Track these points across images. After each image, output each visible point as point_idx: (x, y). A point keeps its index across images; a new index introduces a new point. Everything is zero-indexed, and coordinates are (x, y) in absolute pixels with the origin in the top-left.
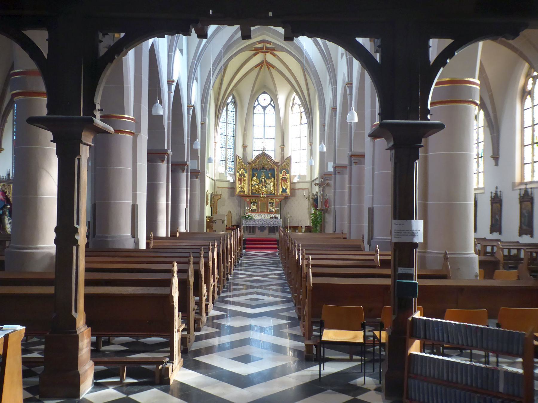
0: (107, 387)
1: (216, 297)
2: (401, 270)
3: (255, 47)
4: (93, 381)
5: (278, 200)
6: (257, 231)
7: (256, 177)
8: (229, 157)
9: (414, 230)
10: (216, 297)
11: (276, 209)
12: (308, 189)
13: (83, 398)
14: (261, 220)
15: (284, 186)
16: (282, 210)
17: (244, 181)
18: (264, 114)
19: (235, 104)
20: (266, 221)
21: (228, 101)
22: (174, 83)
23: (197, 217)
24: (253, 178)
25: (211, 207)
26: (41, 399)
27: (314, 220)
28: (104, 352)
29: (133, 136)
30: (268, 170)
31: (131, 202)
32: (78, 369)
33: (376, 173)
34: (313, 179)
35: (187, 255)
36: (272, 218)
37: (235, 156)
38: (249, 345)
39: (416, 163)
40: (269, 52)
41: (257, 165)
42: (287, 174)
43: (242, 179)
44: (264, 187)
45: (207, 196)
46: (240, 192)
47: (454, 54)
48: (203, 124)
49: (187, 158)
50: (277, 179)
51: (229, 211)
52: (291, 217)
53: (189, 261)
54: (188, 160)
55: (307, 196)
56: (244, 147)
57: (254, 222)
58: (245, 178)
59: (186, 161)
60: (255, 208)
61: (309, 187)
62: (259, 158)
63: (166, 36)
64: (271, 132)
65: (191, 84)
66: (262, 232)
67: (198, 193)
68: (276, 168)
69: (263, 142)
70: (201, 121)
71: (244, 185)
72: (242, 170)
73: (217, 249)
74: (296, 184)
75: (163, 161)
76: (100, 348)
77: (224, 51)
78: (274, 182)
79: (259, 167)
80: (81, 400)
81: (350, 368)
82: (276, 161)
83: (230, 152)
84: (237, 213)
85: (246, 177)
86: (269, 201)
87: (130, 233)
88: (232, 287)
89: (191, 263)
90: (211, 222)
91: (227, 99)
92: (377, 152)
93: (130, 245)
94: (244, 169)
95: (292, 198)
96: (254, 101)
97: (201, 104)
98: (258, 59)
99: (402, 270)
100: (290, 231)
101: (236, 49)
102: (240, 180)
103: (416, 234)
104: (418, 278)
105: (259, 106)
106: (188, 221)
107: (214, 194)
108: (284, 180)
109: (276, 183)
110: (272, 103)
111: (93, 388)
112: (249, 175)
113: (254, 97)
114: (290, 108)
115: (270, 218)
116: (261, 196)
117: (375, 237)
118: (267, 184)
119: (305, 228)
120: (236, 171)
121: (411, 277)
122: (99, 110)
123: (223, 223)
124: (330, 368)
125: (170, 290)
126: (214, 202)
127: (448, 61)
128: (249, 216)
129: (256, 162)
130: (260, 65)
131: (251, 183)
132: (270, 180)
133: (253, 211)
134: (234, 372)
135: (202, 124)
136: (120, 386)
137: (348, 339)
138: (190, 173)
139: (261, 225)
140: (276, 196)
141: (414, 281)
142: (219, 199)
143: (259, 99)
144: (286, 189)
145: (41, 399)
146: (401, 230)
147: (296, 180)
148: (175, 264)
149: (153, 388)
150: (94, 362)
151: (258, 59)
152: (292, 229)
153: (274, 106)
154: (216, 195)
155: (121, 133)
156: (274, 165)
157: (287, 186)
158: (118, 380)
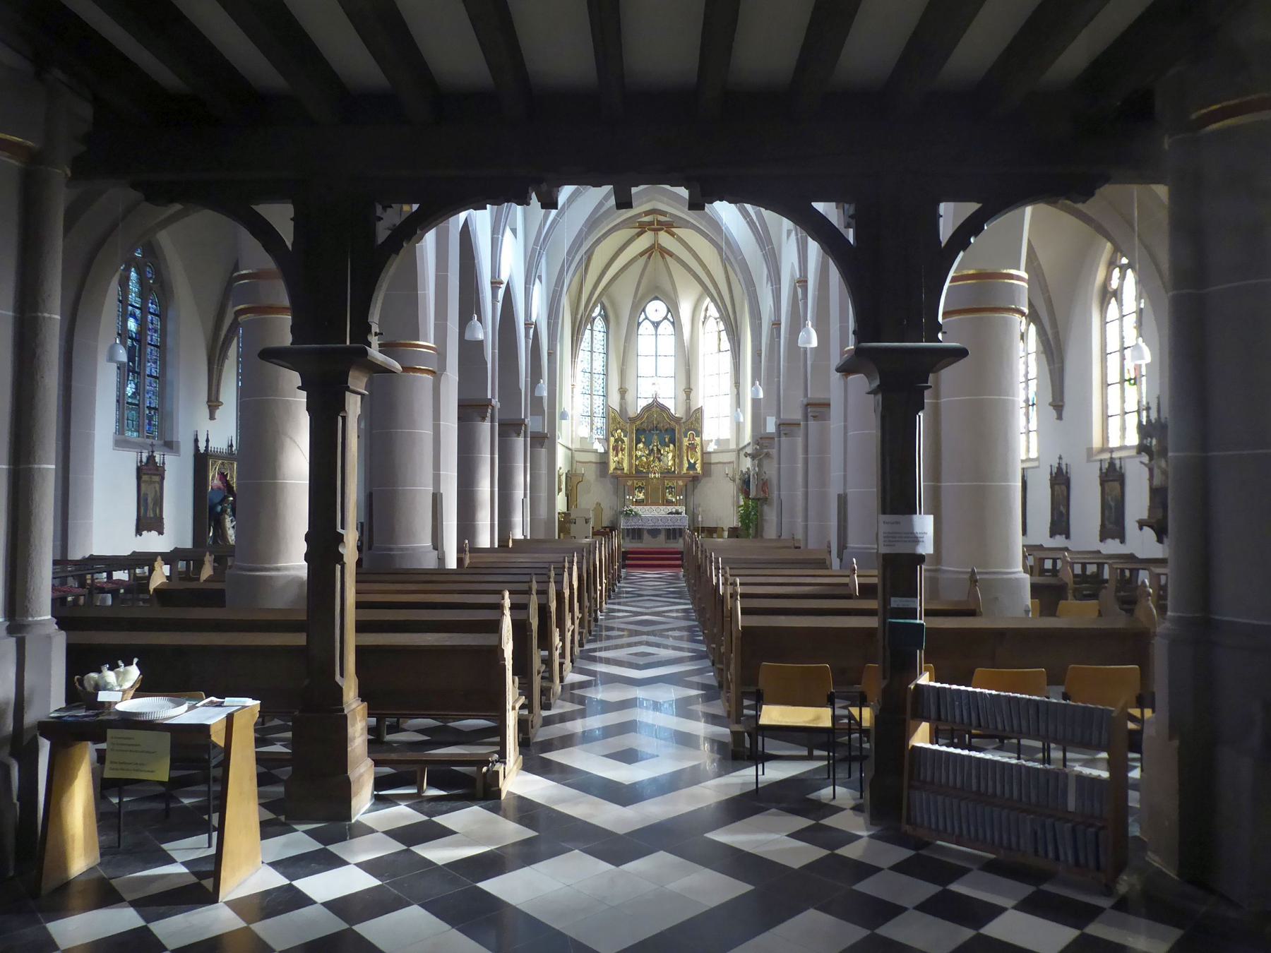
1: (577, 650)
2: (896, 602)
3: (639, 222)
4: (372, 793)
5: (681, 483)
6: (646, 536)
7: (644, 443)
10: (577, 650)
11: (678, 498)
12: (733, 462)
13: (357, 821)
17: (622, 450)
18: (656, 335)
19: (606, 318)
21: (594, 315)
22: (501, 286)
25: (567, 496)
26: (287, 822)
28: (389, 743)
31: (431, 489)
33: (850, 433)
34: (741, 446)
35: (526, 578)
36: (671, 513)
37: (607, 407)
39: (920, 417)
40: (662, 229)
41: (644, 422)
42: (696, 438)
43: (619, 448)
46: (616, 469)
48: (551, 355)
49: (525, 412)
52: (703, 511)
55: (730, 475)
56: (623, 392)
60: (641, 496)
63: (488, 206)
64: (668, 366)
67: (544, 471)
68: (677, 427)
69: (654, 384)
70: (548, 350)
72: (619, 431)
78: (674, 451)
82: (677, 415)
83: (599, 401)
85: (626, 443)
88: (604, 633)
91: (592, 310)
93: (430, 562)
98: (644, 242)
103: (921, 539)
104: (925, 616)
106: (527, 520)
108: (692, 447)
109: (677, 452)
111: (373, 804)
112: (631, 440)
113: (638, 307)
115: (668, 514)
118: (662, 455)
120: (610, 433)
121: (912, 613)
122: (376, 334)
123: (586, 523)
124: (775, 772)
128: (631, 511)
129: (643, 417)
130: (649, 252)
132: (667, 449)
133: (638, 503)
135: (549, 354)
136: (417, 801)
141: (918, 621)
143: (647, 309)
144: (695, 463)
145: (287, 822)
147: (711, 448)
148: (507, 594)
151: (644, 242)
153: (672, 320)
154: (576, 475)
155: (413, 372)
156: (673, 423)
158: (415, 791)
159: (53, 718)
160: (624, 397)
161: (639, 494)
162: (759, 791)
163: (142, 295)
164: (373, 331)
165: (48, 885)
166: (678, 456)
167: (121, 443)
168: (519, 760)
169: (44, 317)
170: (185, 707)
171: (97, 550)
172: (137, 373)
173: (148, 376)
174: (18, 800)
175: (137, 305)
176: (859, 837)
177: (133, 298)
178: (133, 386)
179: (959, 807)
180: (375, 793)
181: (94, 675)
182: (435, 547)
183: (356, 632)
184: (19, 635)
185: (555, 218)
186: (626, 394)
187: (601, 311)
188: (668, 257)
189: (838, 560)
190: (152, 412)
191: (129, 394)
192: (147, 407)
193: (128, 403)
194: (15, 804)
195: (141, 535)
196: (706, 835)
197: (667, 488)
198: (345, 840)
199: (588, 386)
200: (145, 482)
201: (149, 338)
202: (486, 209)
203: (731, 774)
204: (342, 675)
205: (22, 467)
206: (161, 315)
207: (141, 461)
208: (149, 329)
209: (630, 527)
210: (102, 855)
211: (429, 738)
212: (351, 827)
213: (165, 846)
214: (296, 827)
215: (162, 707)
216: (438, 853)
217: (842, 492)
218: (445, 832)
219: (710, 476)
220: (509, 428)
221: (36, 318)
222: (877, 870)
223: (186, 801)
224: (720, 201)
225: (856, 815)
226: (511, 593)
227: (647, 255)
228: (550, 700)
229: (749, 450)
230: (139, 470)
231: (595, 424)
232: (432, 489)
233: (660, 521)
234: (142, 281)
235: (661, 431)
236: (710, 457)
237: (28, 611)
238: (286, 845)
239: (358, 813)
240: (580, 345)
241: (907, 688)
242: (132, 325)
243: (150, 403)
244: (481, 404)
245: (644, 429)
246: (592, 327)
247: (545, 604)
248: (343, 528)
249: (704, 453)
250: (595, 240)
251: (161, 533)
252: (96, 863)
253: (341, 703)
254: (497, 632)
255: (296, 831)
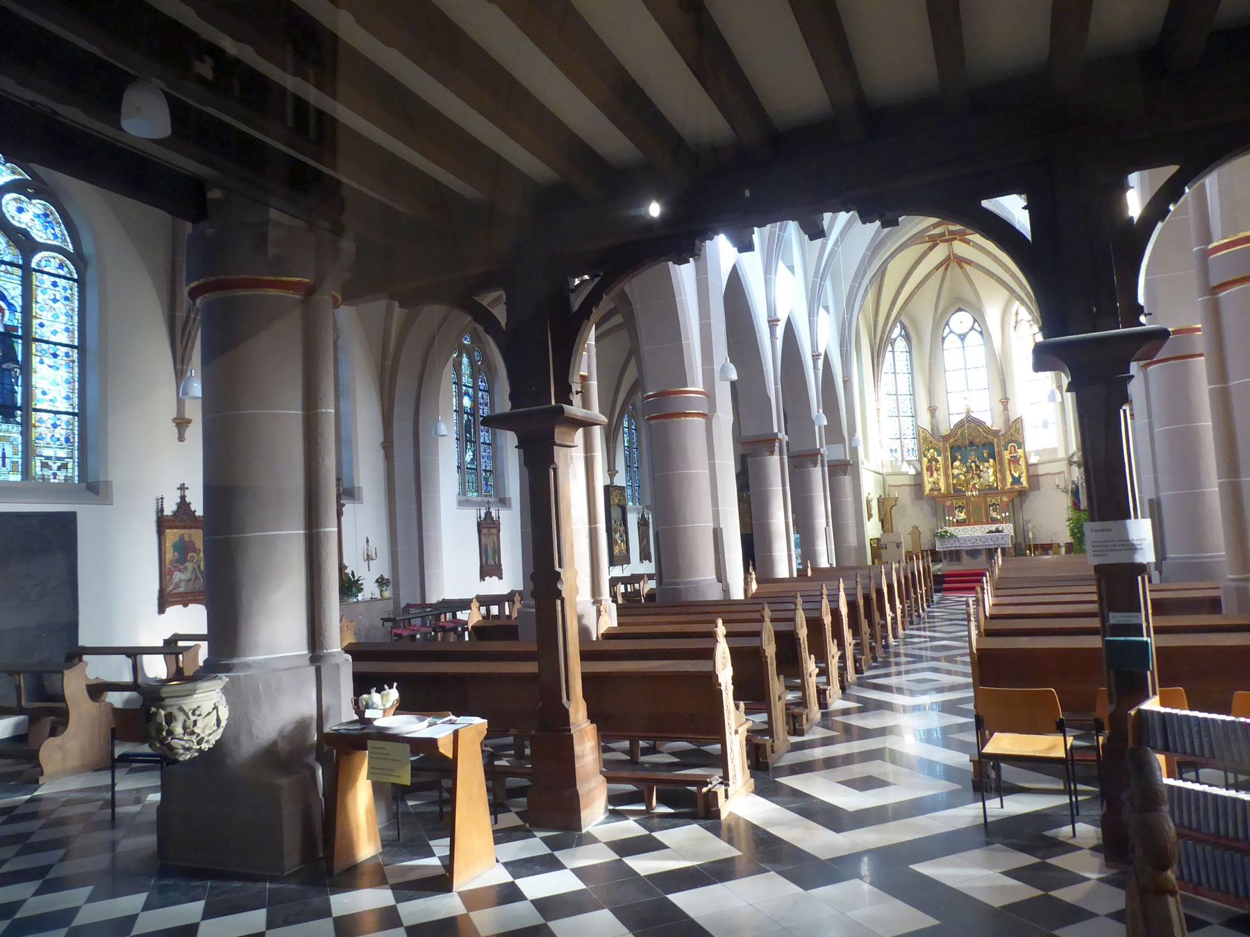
0: (625, 817)
1: (851, 676)
2: (1115, 618)
3: (928, 236)
4: (606, 807)
5: (1005, 499)
6: (965, 557)
7: (960, 461)
8: (906, 432)
9: (1133, 540)
10: (851, 676)
11: (1003, 515)
12: (1063, 472)
13: (588, 833)
14: (970, 539)
15: (1016, 472)
16: (1016, 516)
17: (937, 470)
18: (964, 347)
19: (907, 338)
20: (981, 538)
21: (893, 336)
22: (778, 323)
23: (852, 540)
24: (954, 464)
25: (882, 521)
26: (531, 829)
27: (1075, 531)
28: (643, 763)
29: (706, 419)
30: (980, 447)
31: (711, 525)
32: (576, 787)
33: (1156, 430)
34: (1070, 453)
35: (758, 607)
36: (991, 532)
37: (917, 428)
38: (881, 760)
39: (1125, 411)
40: (956, 239)
41: (958, 439)
42: (1019, 451)
43: (934, 468)
44: (976, 477)
45: (868, 502)
46: (932, 490)
47: (1183, 193)
48: (847, 382)
49: (820, 442)
50: (999, 461)
51: (914, 526)
52: (1034, 527)
53: (763, 617)
54: (821, 446)
55: (1062, 486)
56: (932, 410)
57: (957, 542)
58: (938, 466)
59: (818, 447)
60: (963, 516)
61: (1065, 470)
62: (961, 427)
63: (691, 259)
64: (981, 377)
65: (815, 319)
66: (976, 559)
67: (849, 498)
68: (995, 440)
69: (965, 398)
70: (843, 377)
71: (938, 479)
72: (932, 451)
73: (846, 595)
74: (1038, 466)
75: (772, 453)
76: (638, 759)
77: (870, 254)
78: (994, 467)
79: (962, 443)
80: (585, 834)
81: (1059, 806)
82: (994, 428)
83: (907, 424)
84: (930, 530)
85: (941, 462)
86: (988, 501)
87: (714, 573)
88: (893, 660)
89: (767, 619)
90: (878, 548)
91: (891, 332)
92: (1153, 390)
93: (714, 594)
94: (935, 449)
95: (1034, 492)
96: (943, 327)
97: (841, 347)
98: (939, 253)
99: (1116, 617)
100: (1037, 553)
101: (892, 246)
102: (929, 469)
103: (1138, 547)
104: (1155, 633)
105: (973, 331)
106: (831, 549)
107: (885, 499)
108: (1015, 460)
109: (999, 467)
110: (976, 326)
111: (607, 818)
112: (946, 459)
113: (941, 321)
114: (1012, 329)
115: (988, 533)
116: (970, 494)
117: (1169, 555)
118: (981, 471)
119: (1066, 547)
120: (922, 454)
121: (1137, 630)
122: (577, 393)
123: (898, 547)
124: (1015, 806)
125: (712, 665)
126: (886, 512)
127: (1172, 207)
128: (946, 532)
129: (956, 434)
130: (945, 263)
131: (950, 472)
132: (986, 464)
133: (960, 523)
134: (834, 804)
135: (845, 382)
136: (646, 818)
137: (1039, 751)
138: (828, 467)
139: (971, 546)
140: (1003, 491)
141: (1145, 639)
142: (893, 507)
143: (950, 323)
144: (1020, 477)
145: (531, 829)
146: (1106, 541)
147: (1033, 459)
148: (720, 622)
149: (692, 824)
150: (605, 777)
151: (939, 253)
152: (1039, 549)
153: (980, 330)
154: (889, 499)
155: (684, 417)
156: (990, 437)
157: (1021, 472)
158: (644, 808)
159: (333, 730)
160: (1007, 407)
161: (960, 514)
162: (989, 826)
163: (473, 376)
164: (574, 390)
165: (338, 866)
166: (1000, 470)
167: (463, 503)
168: (748, 783)
169: (322, 413)
170: (426, 723)
171: (449, 595)
172: (473, 442)
173: (482, 443)
174: (323, 796)
175: (470, 385)
176: (1086, 879)
177: (466, 379)
178: (471, 454)
179: (1195, 849)
180: (611, 807)
181: (365, 696)
182: (719, 580)
183: (581, 660)
184: (317, 664)
185: (832, 249)
186: (937, 413)
187: (901, 331)
188: (967, 267)
189: (1157, 573)
190: (488, 475)
191: (468, 461)
192: (483, 470)
193: (467, 468)
194: (321, 799)
195: (484, 580)
196: (910, 866)
197: (990, 506)
198: (571, 847)
199: (894, 408)
200: (485, 534)
201: (481, 411)
202: (689, 262)
203: (966, 806)
204: (568, 698)
205: (314, 531)
206: (489, 391)
207: (480, 517)
208: (481, 404)
209: (945, 549)
210: (383, 846)
211: (679, 760)
212: (581, 836)
213: (432, 843)
214: (536, 833)
215: (409, 723)
216: (644, 865)
217: (1153, 496)
218: (660, 846)
219: (1039, 490)
220: (801, 461)
221: (317, 413)
222: (1091, 915)
223: (410, 803)
224: (870, 223)
225: (1093, 856)
226: (724, 623)
227: (943, 267)
228: (802, 726)
229: (1075, 459)
230: (479, 524)
231: (906, 446)
232: (712, 524)
233: (989, 540)
234: (472, 363)
235: (978, 447)
236: (1037, 468)
237: (323, 645)
238: (522, 849)
239: (589, 825)
240: (882, 368)
241: (1127, 716)
242: (467, 402)
243: (486, 467)
244: (767, 439)
245: (959, 446)
246: (893, 348)
247: (793, 631)
248: (560, 567)
249: (1028, 466)
250: (881, 262)
251: (501, 578)
252: (378, 852)
253: (568, 724)
254: (712, 659)
255: (535, 836)
